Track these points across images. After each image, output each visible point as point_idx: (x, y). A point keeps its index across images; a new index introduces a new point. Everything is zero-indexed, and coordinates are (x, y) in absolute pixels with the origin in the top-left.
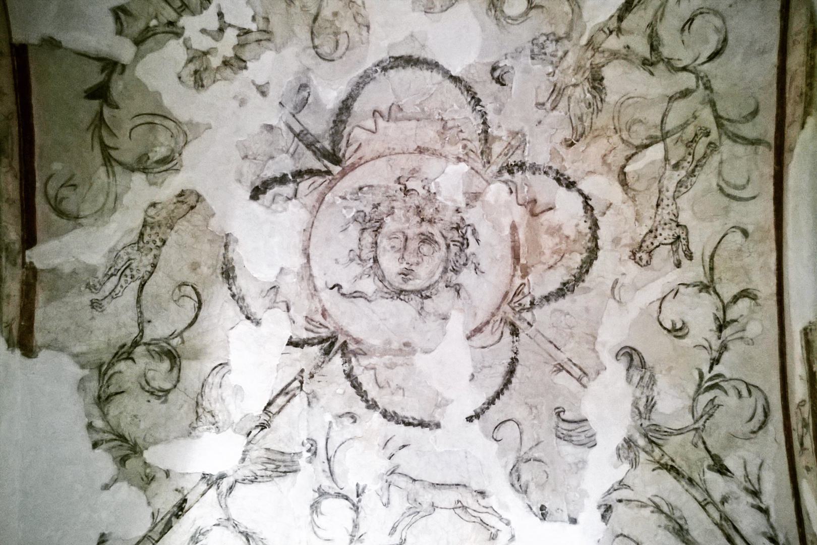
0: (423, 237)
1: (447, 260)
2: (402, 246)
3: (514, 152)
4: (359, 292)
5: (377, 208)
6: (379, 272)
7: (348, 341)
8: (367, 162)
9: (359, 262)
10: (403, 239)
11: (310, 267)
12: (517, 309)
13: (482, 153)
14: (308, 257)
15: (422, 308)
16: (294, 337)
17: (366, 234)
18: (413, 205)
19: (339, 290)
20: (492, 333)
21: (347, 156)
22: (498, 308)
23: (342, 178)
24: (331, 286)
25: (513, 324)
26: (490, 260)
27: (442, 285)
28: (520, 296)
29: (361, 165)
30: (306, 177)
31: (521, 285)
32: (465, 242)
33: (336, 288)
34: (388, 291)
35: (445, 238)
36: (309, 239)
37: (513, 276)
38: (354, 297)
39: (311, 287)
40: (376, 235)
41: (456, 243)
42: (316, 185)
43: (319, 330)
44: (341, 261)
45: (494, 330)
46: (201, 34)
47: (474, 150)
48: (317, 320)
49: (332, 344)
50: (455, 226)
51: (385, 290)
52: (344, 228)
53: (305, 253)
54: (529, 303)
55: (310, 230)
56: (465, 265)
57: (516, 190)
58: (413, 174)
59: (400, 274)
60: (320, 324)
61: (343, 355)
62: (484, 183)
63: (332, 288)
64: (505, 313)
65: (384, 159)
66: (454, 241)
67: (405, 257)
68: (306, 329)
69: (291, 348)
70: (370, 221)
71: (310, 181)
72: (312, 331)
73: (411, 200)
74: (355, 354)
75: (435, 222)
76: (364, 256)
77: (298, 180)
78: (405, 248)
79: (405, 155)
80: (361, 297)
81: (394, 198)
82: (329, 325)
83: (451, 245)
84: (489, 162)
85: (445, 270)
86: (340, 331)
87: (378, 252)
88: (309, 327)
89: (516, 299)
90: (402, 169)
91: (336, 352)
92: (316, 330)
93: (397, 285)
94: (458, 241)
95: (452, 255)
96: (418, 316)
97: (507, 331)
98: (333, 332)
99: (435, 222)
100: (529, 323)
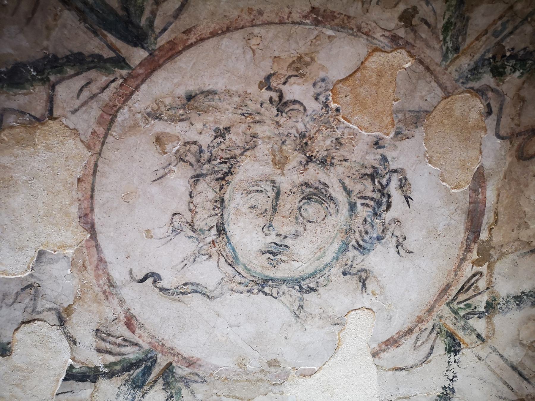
0: (308, 190)
1: (349, 231)
2: (269, 206)
3: (516, 28)
4: (192, 284)
5: (223, 136)
6: (228, 249)
7: (174, 364)
8: (202, 40)
9: (192, 234)
10: (272, 194)
11: (97, 246)
12: (462, 313)
13: (446, 28)
14: (92, 229)
15: (301, 307)
16: (77, 366)
17: (202, 186)
18: (293, 131)
19: (155, 282)
20: (415, 348)
21: (158, 23)
22: (430, 310)
23: (148, 75)
24: (141, 277)
25: (451, 335)
26: (424, 232)
27: (337, 270)
28: (471, 292)
29: (191, 45)
30: (70, 71)
31: (474, 275)
32: (384, 200)
33: (150, 280)
34: (243, 280)
35: (348, 192)
36: (92, 197)
37: (463, 260)
38: (183, 293)
39: (103, 281)
40: (221, 188)
41: (367, 201)
42: (94, 88)
43: (123, 350)
44: (159, 232)
45: (419, 343)
46: (266, 91)
47: (431, 20)
48: (117, 334)
49: (148, 370)
50: (369, 171)
51: (238, 278)
52: (161, 173)
53: (86, 223)
54: (484, 304)
55: (91, 178)
56: (379, 239)
57: (501, 109)
58: (297, 69)
59: (264, 253)
60: (124, 340)
61: (167, 386)
62: (439, 92)
63: (141, 281)
64: (441, 318)
65: (237, 35)
66: (364, 198)
67: (274, 223)
68: (99, 351)
69: (74, 384)
70: (209, 161)
71: (78, 82)
72: (110, 353)
73: (290, 123)
74: (187, 382)
75: (332, 164)
76: (199, 224)
77: (52, 78)
78: (275, 208)
79: (286, 27)
80: (195, 292)
81: (257, 118)
82: (140, 342)
83: (359, 205)
84: (456, 49)
85: (344, 248)
86: (159, 348)
87: (225, 217)
88: (103, 345)
89: (461, 297)
90: (276, 59)
91: (155, 382)
92: (116, 349)
93: (259, 270)
94: (372, 199)
95: (360, 220)
96: (293, 319)
97: (441, 346)
98: (149, 351)
99: (332, 164)
100: (479, 336)
